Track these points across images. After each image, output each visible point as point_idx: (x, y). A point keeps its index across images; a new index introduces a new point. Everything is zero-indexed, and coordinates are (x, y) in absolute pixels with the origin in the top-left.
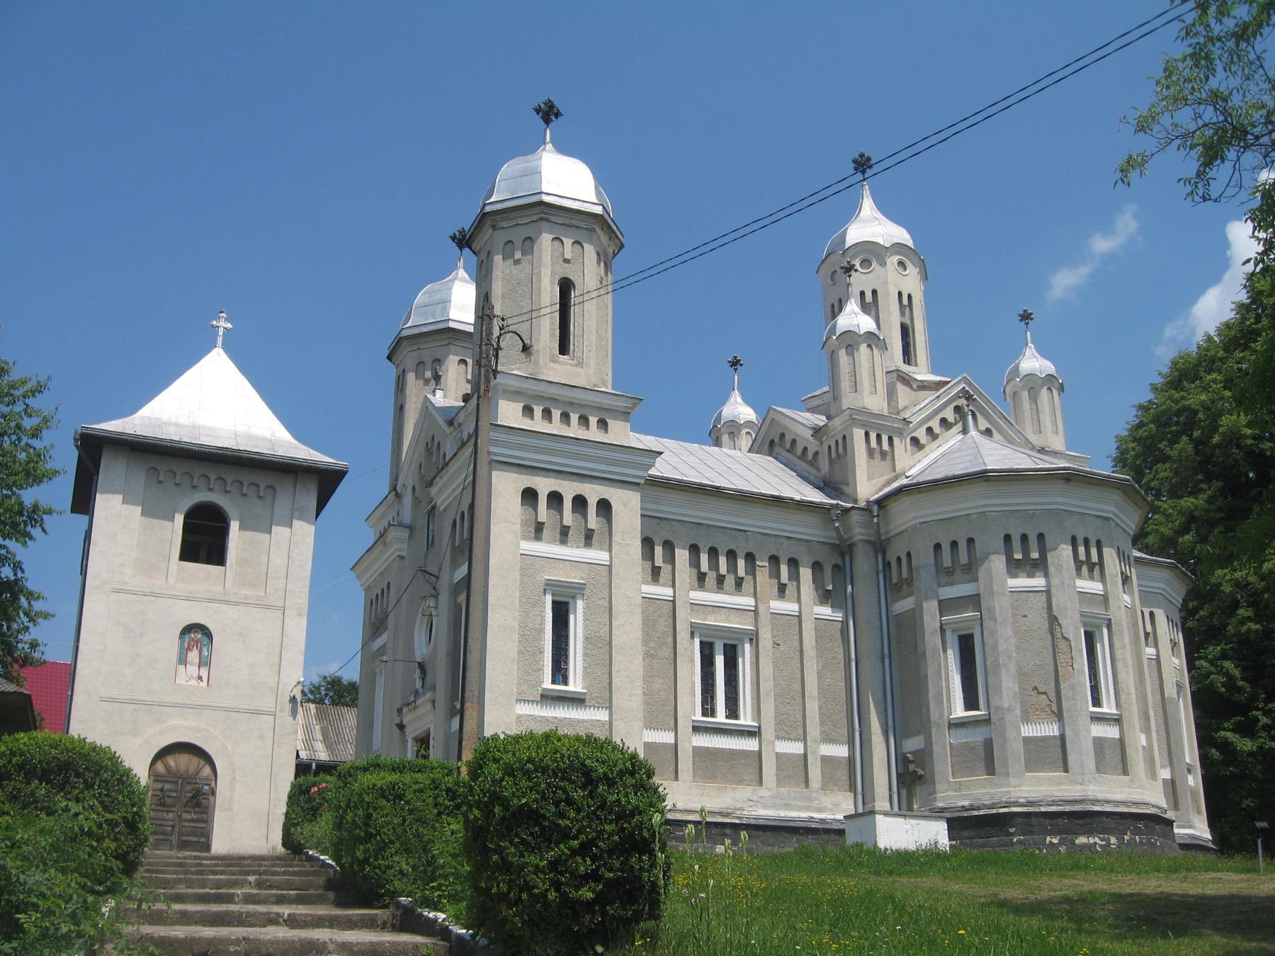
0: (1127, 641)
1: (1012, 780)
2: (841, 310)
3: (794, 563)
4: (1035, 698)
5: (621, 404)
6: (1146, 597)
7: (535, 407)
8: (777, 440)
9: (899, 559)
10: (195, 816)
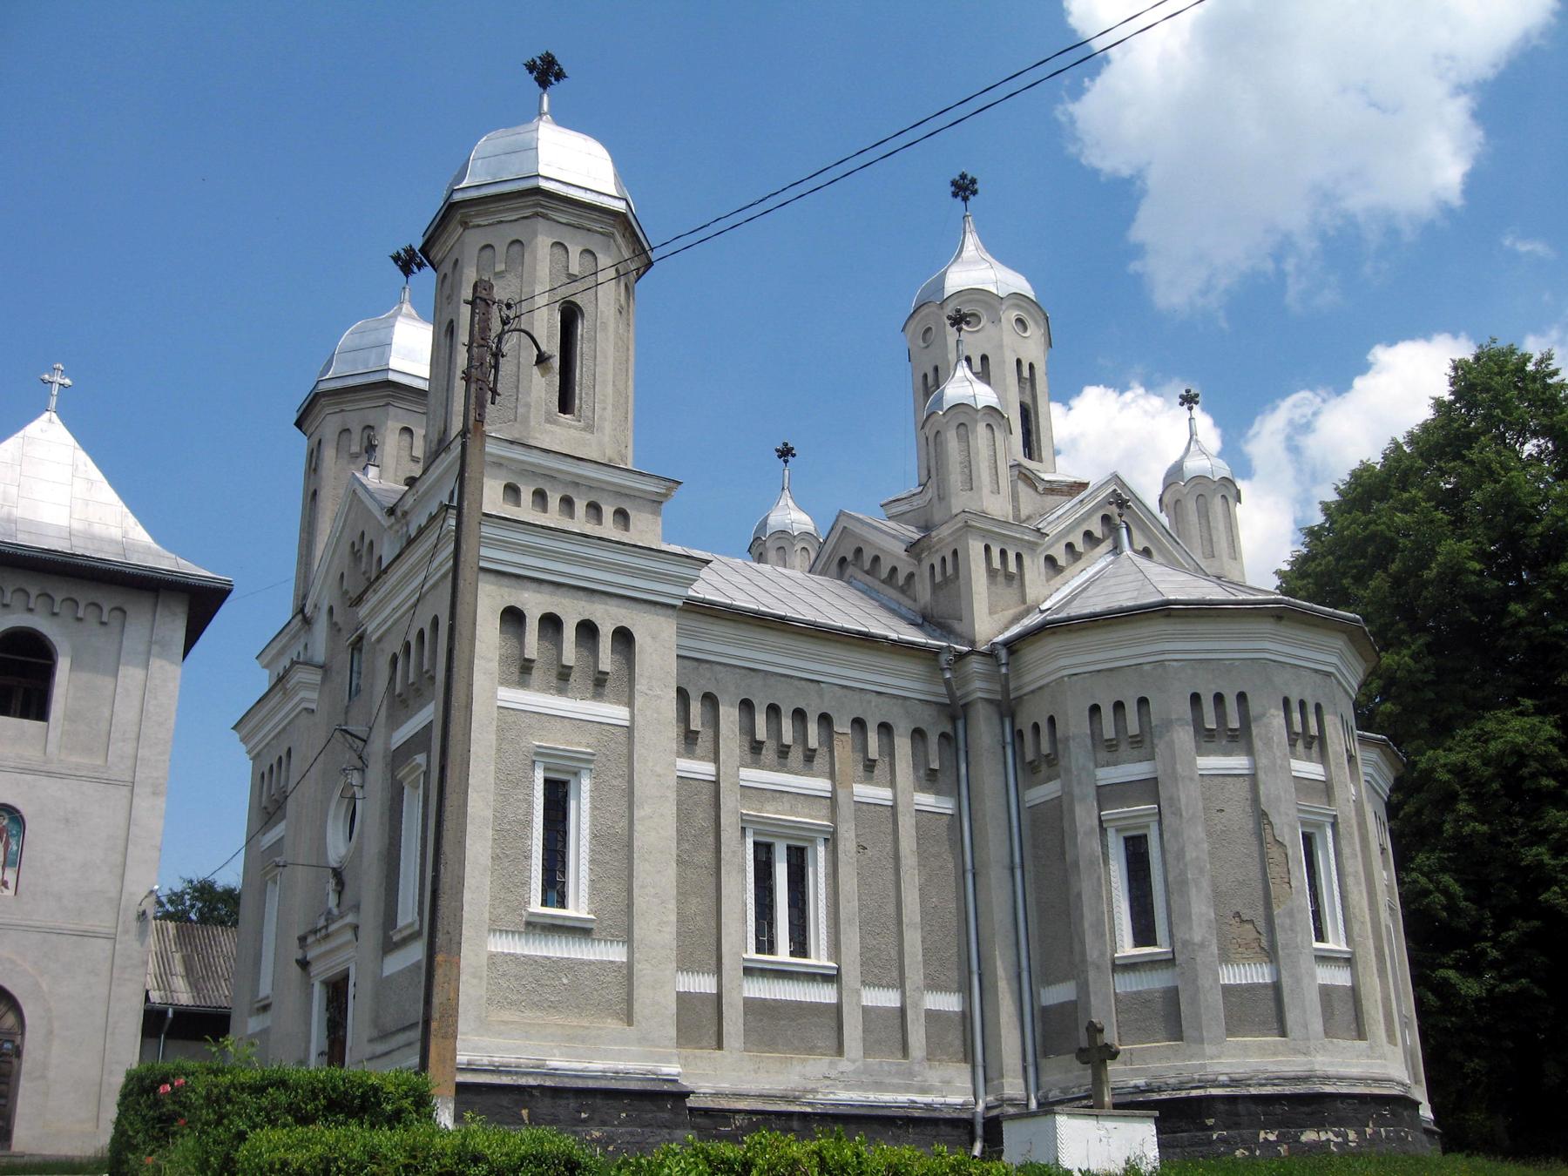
1: (1209, 1049)
8: (850, 557)
9: (1036, 727)
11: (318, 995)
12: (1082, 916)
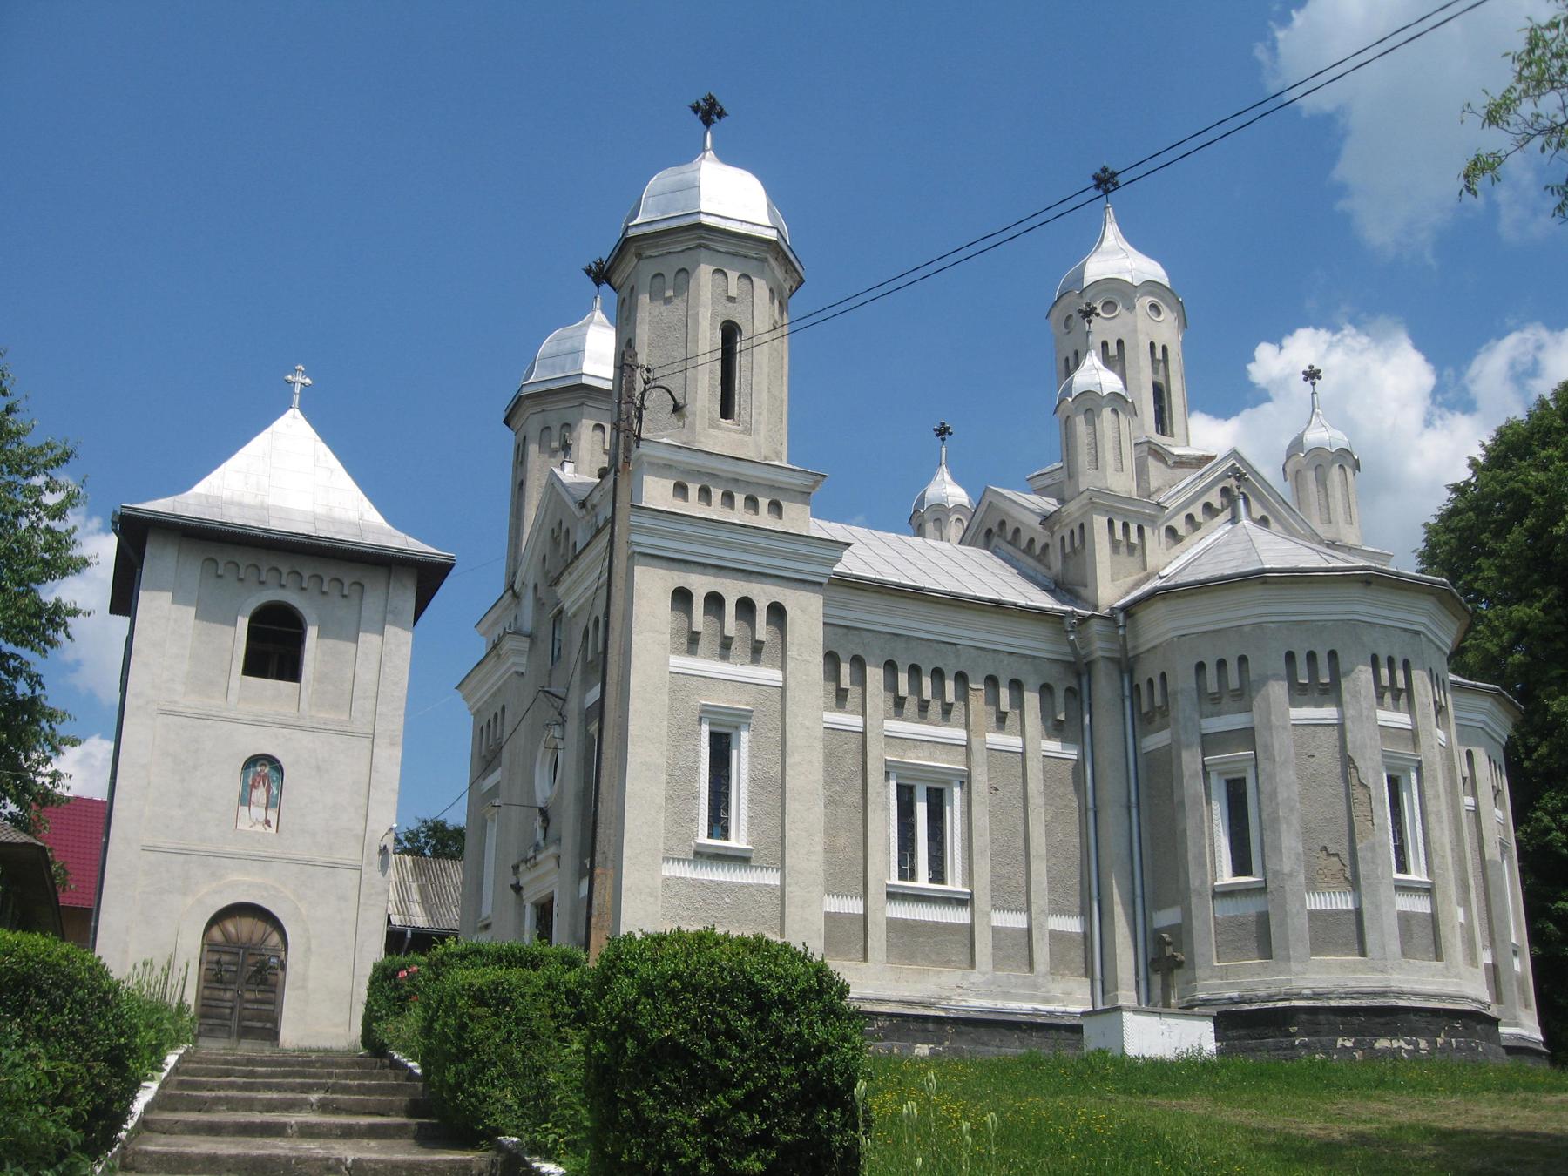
0: (1441, 790)
1: (1294, 966)
2: (1077, 366)
3: (1016, 686)
4: (1323, 860)
5: (800, 481)
6: (1465, 733)
7: (690, 486)
8: (995, 529)
9: (1150, 682)
10: (259, 996)
11: (529, 915)
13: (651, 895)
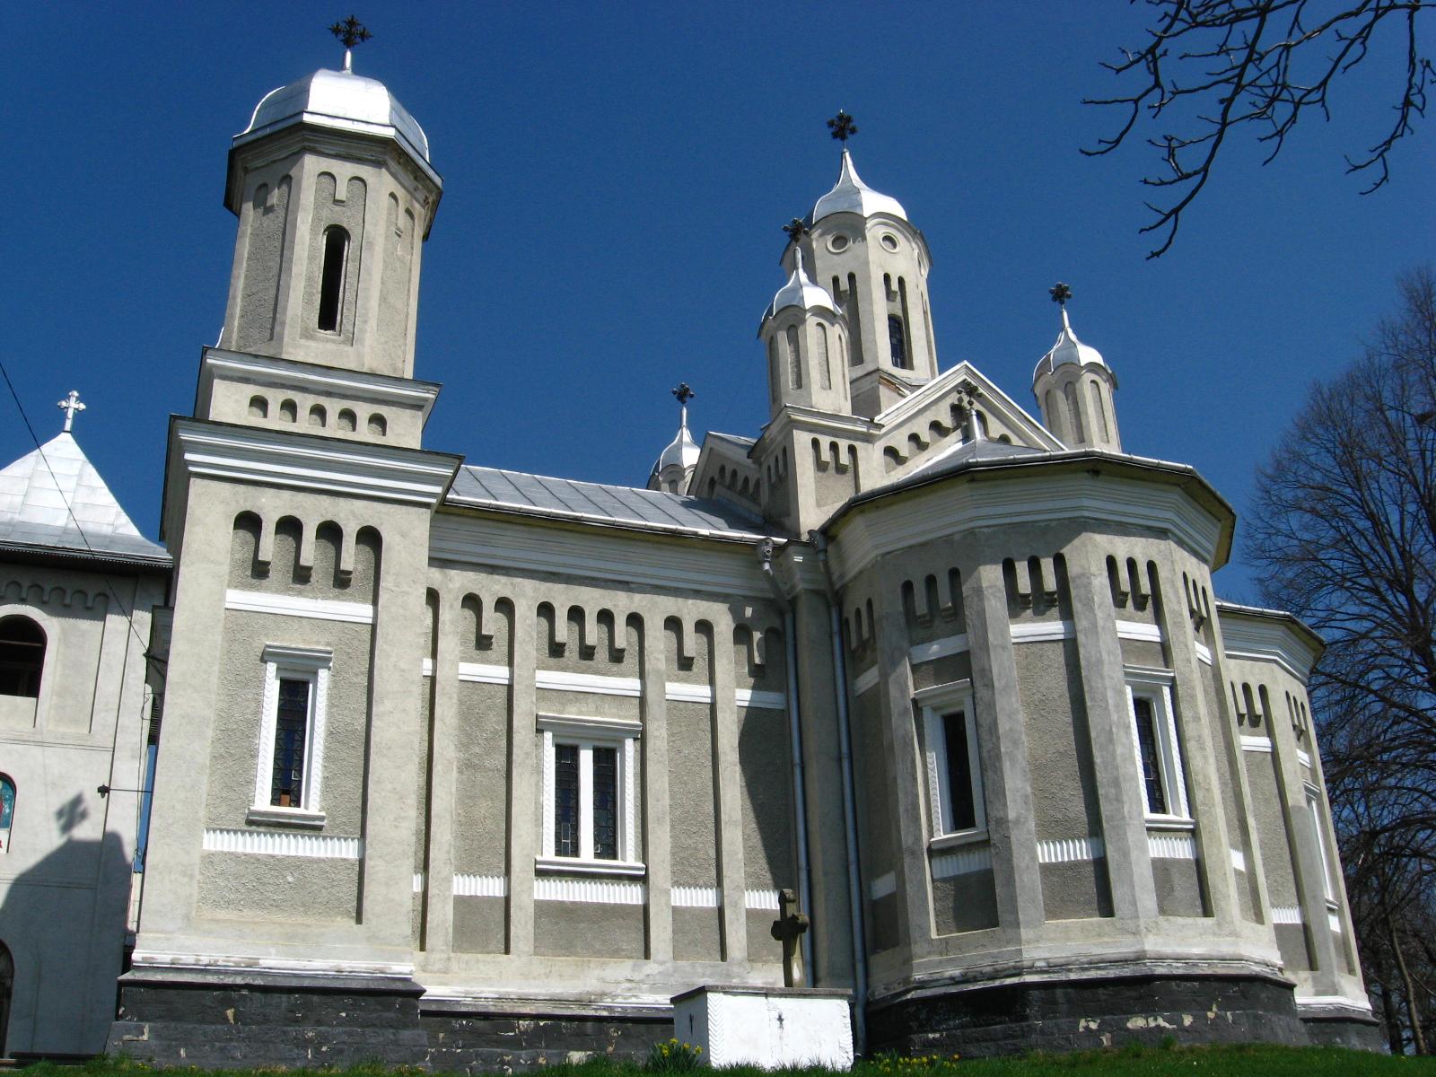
0: (1202, 709)
9: (858, 612)
12: (897, 800)
13: (184, 874)
